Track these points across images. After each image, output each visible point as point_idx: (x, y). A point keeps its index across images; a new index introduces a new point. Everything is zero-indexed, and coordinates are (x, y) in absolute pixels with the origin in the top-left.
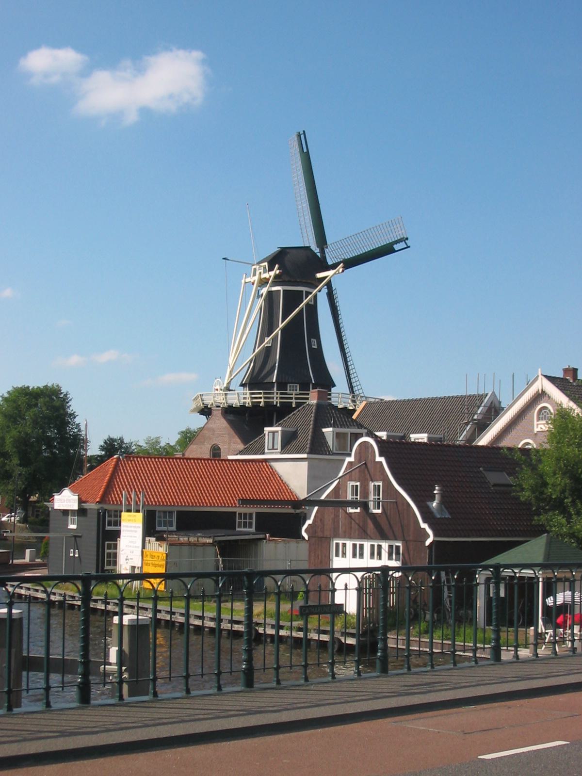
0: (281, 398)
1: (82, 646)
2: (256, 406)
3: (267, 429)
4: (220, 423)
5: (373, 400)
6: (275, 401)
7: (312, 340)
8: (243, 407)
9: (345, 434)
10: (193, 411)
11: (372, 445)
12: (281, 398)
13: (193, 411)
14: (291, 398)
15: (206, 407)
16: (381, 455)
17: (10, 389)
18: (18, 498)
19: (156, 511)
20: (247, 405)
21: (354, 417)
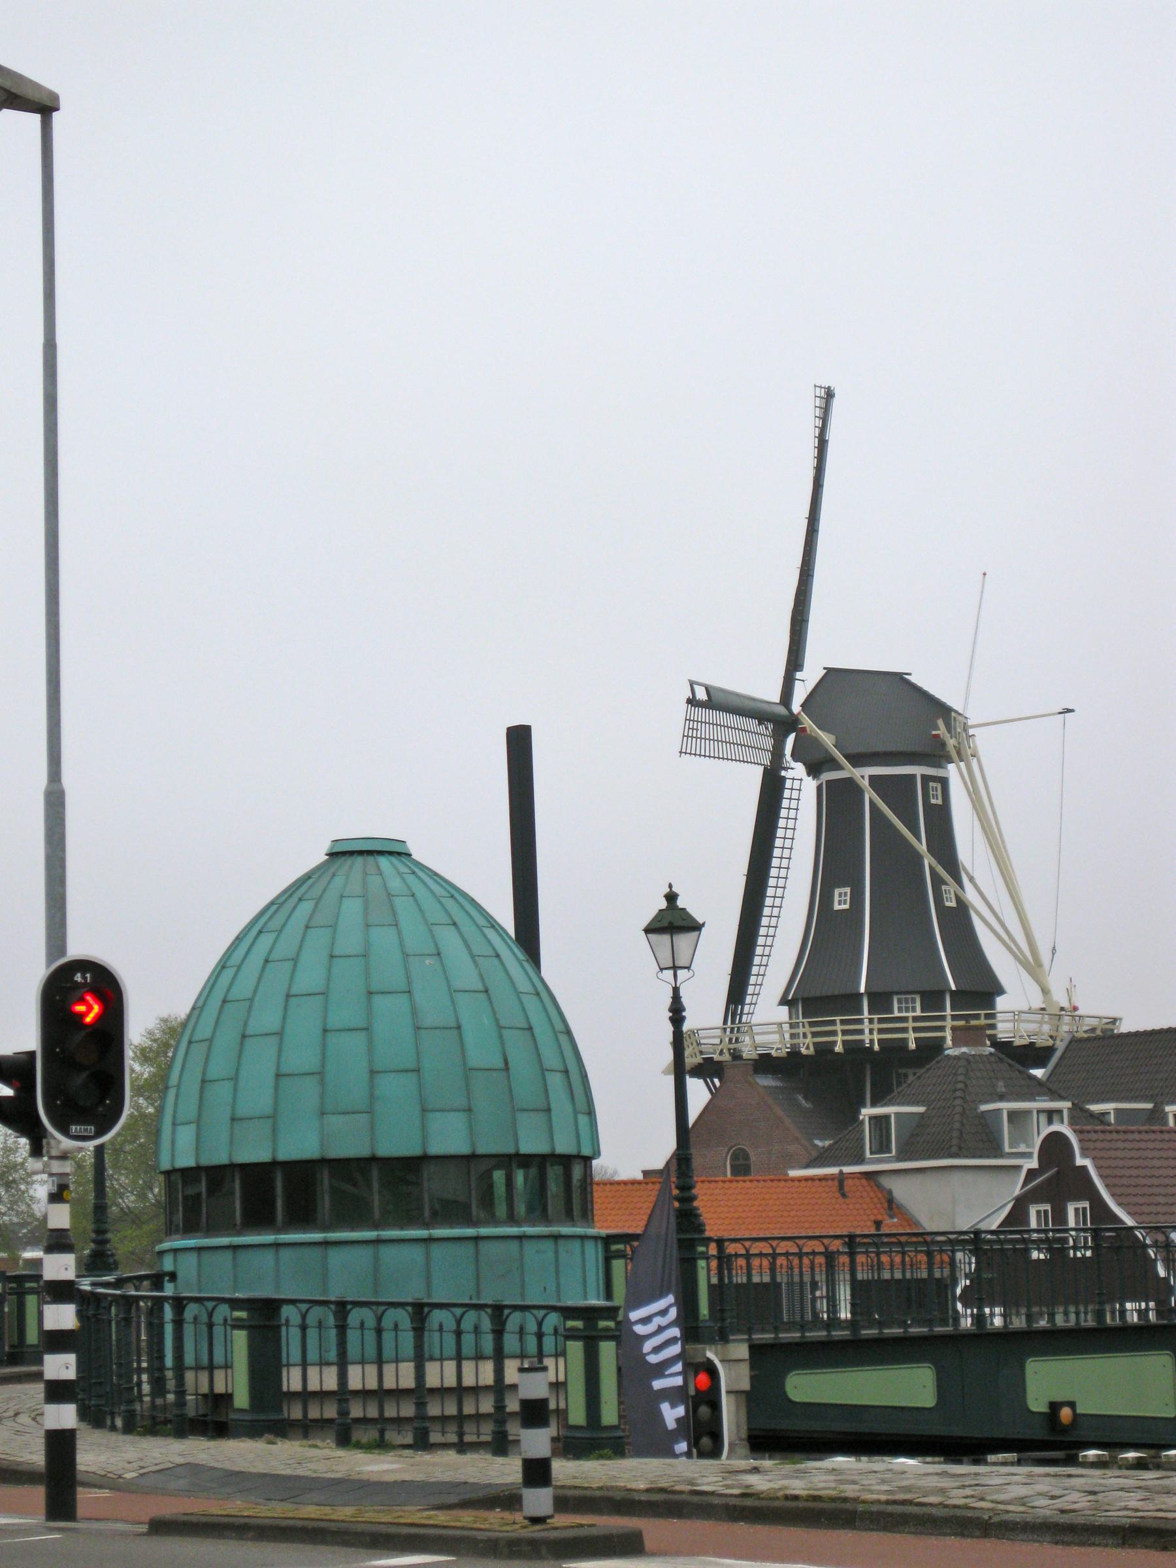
2: (824, 1050)
6: (866, 1037)
8: (794, 1054)
20: (803, 1051)
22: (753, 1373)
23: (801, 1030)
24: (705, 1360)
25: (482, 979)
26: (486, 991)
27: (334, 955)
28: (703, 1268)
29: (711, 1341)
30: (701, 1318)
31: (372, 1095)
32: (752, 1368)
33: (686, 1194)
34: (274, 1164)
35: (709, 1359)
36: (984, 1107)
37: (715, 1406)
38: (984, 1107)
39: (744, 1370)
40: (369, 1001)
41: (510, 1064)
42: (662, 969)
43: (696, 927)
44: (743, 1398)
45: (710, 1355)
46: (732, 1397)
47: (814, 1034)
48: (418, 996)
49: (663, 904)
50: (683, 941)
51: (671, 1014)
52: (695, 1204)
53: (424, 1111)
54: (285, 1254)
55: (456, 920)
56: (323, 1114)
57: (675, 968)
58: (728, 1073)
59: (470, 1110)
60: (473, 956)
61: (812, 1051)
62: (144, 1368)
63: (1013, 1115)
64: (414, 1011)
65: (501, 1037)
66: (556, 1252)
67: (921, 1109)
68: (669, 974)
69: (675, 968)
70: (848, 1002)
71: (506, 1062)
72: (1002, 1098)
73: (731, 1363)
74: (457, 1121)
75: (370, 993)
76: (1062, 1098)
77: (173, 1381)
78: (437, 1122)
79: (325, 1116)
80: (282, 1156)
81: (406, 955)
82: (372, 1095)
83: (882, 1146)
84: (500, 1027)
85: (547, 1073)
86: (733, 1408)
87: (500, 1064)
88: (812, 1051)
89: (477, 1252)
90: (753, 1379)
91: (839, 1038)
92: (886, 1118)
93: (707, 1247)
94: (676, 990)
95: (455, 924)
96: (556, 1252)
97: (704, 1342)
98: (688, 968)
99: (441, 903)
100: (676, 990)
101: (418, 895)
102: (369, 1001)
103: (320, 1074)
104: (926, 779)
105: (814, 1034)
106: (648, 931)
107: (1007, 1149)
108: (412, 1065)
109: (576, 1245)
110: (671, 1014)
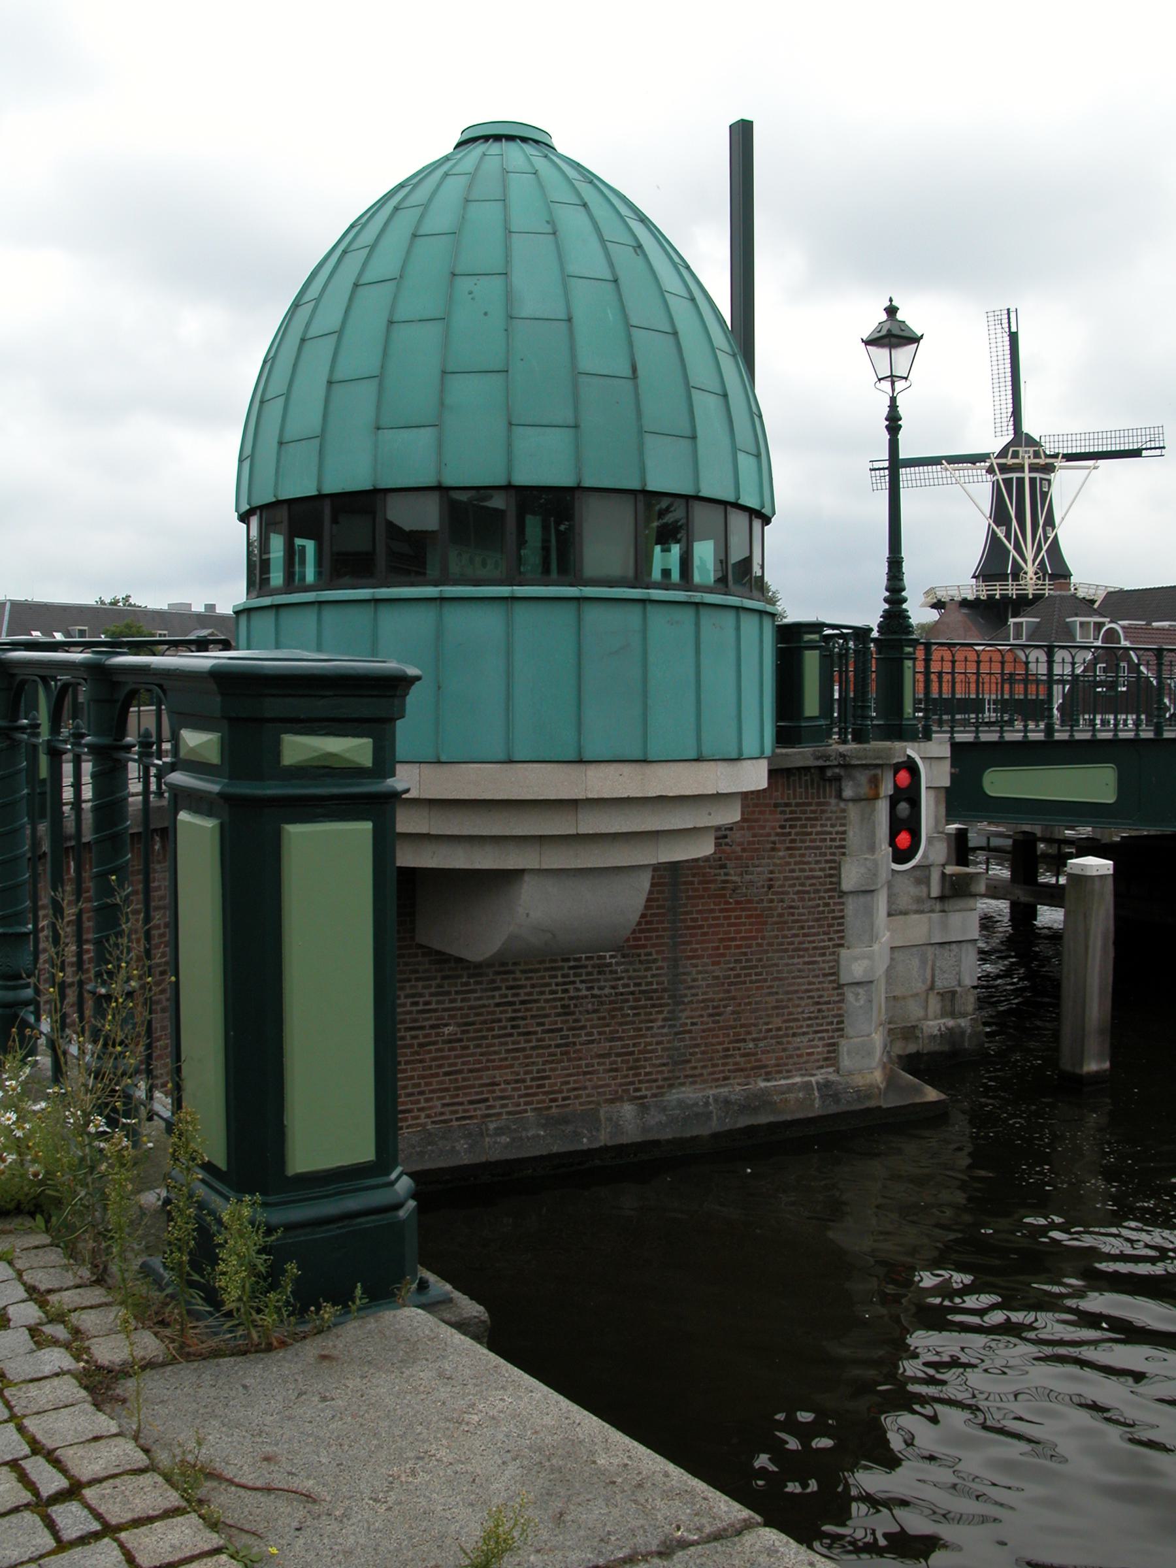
0: (1017, 590)
1: (1036, 920)
2: (991, 598)
3: (1012, 621)
4: (958, 617)
5: (1112, 590)
6: (1010, 592)
7: (299, 542)
8: (978, 599)
9: (1089, 623)
10: (923, 606)
11: (1117, 631)
12: (1017, 590)
13: (923, 606)
14: (996, 590)
15: (939, 601)
16: (1125, 640)
17: (769, 583)
18: (836, 733)
19: (778, 726)
20: (982, 597)
21: (1096, 606)
22: (953, 771)
23: (980, 588)
24: (905, 759)
25: (611, 265)
26: (616, 281)
27: (457, 272)
28: (909, 668)
29: (913, 738)
30: (906, 716)
31: (442, 404)
32: (952, 766)
33: (896, 597)
34: (320, 497)
35: (909, 756)
36: (1068, 620)
37: (915, 803)
38: (1068, 620)
39: (946, 767)
40: (451, 285)
41: (640, 372)
42: (880, 380)
43: (915, 340)
44: (942, 795)
45: (910, 752)
46: (932, 793)
47: (987, 590)
48: (519, 279)
49: (884, 317)
50: (903, 354)
51: (887, 423)
52: (904, 606)
53: (510, 424)
54: (329, 614)
55: (587, 199)
56: (378, 429)
57: (893, 378)
58: (948, 606)
59: (576, 427)
60: (602, 241)
61: (985, 598)
62: (167, 751)
63: (1082, 624)
64: (509, 296)
65: (629, 337)
66: (697, 625)
67: (1038, 620)
68: (886, 385)
69: (893, 378)
70: (1003, 577)
71: (634, 369)
72: (1077, 615)
73: (933, 760)
74: (558, 440)
75: (454, 275)
76: (1105, 617)
77: (130, 776)
78: (526, 440)
79: (380, 431)
80: (328, 489)
81: (508, 232)
82: (442, 404)
83: (1018, 636)
84: (628, 326)
85: (649, 439)
86: (932, 803)
87: (627, 372)
88: (985, 598)
89: (579, 620)
90: (953, 777)
91: (998, 592)
92: (1021, 623)
93: (915, 649)
94: (893, 400)
95: (585, 205)
96: (697, 625)
97: (906, 740)
98: (906, 378)
99: (573, 185)
100: (893, 400)
101: (542, 172)
102: (451, 285)
103: (380, 378)
104: (1041, 479)
105: (987, 590)
106: (868, 342)
107: (1078, 640)
108: (571, 422)
109: (729, 618)
110: (887, 423)
